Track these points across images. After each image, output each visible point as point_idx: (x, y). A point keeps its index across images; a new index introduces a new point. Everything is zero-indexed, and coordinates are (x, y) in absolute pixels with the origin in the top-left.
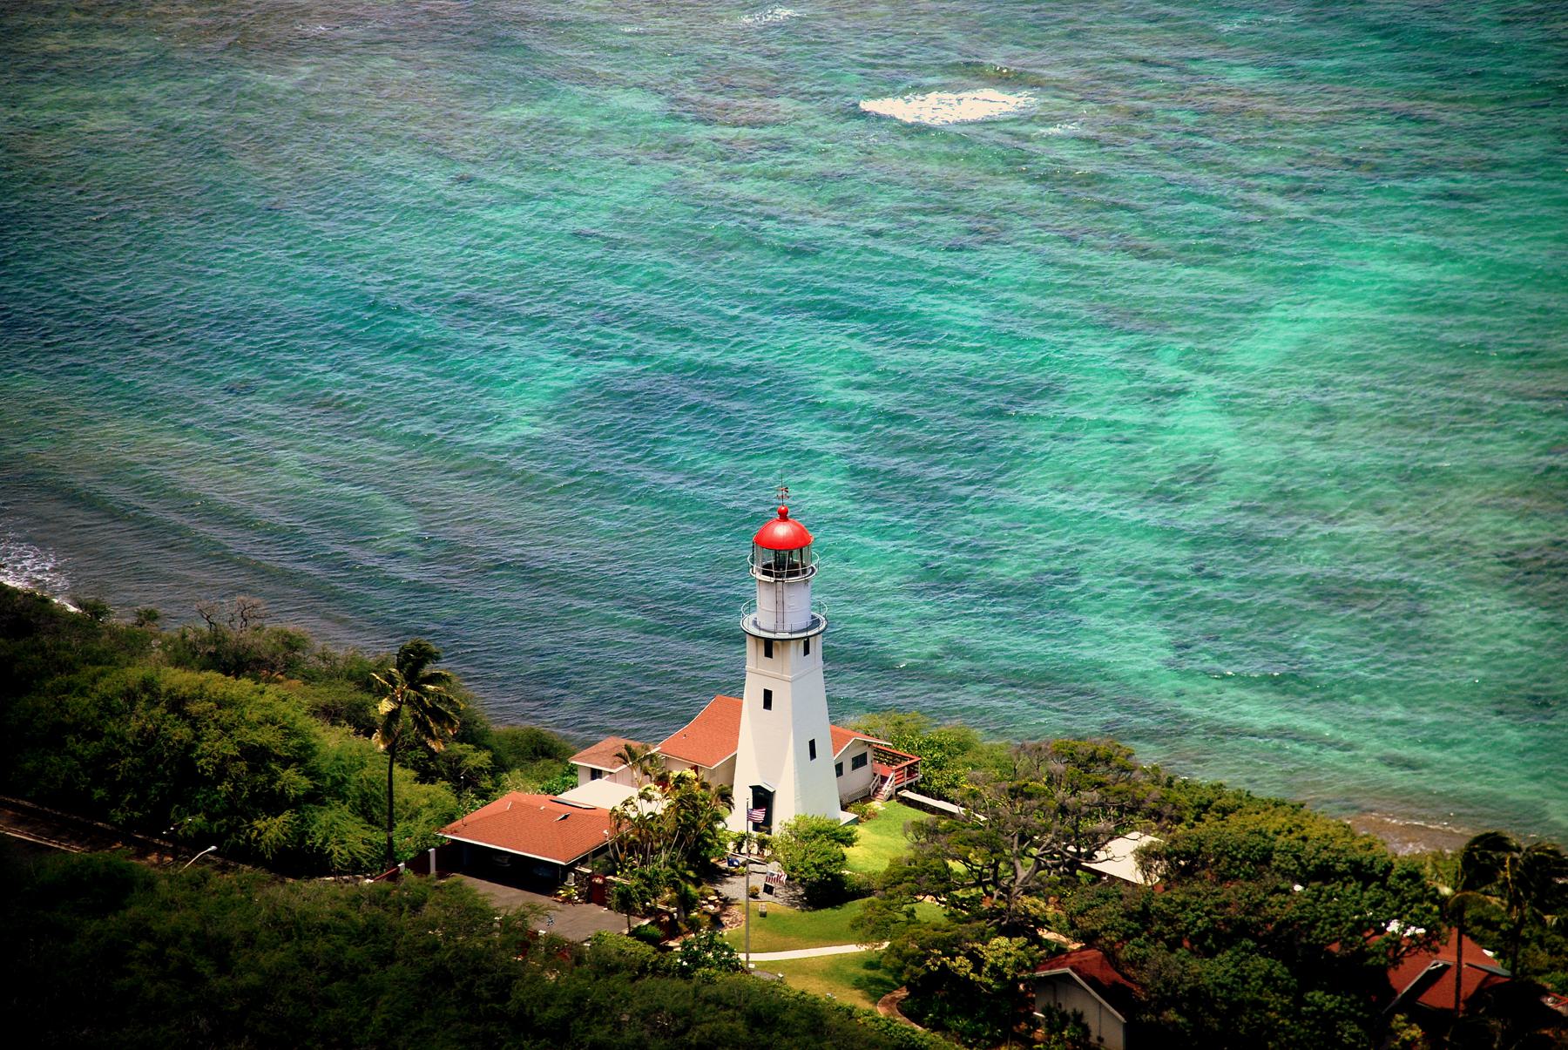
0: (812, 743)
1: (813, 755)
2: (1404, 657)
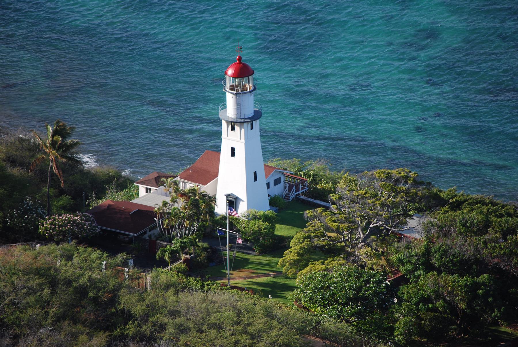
0: (255, 173)
1: (256, 179)
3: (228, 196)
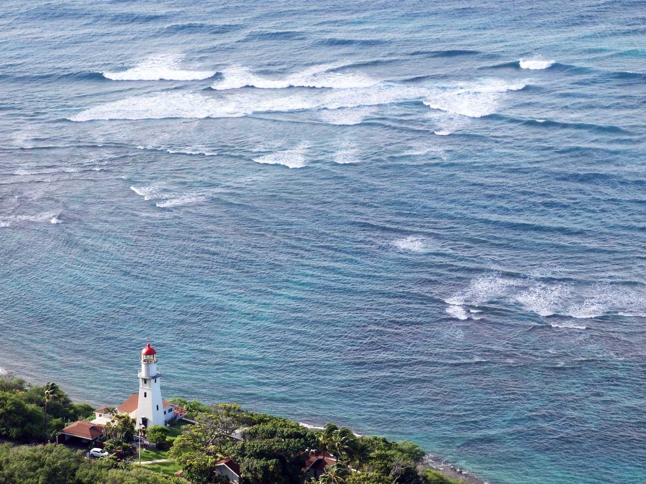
0: (157, 406)
1: (158, 409)
2: (110, 368)
3: (143, 419)
